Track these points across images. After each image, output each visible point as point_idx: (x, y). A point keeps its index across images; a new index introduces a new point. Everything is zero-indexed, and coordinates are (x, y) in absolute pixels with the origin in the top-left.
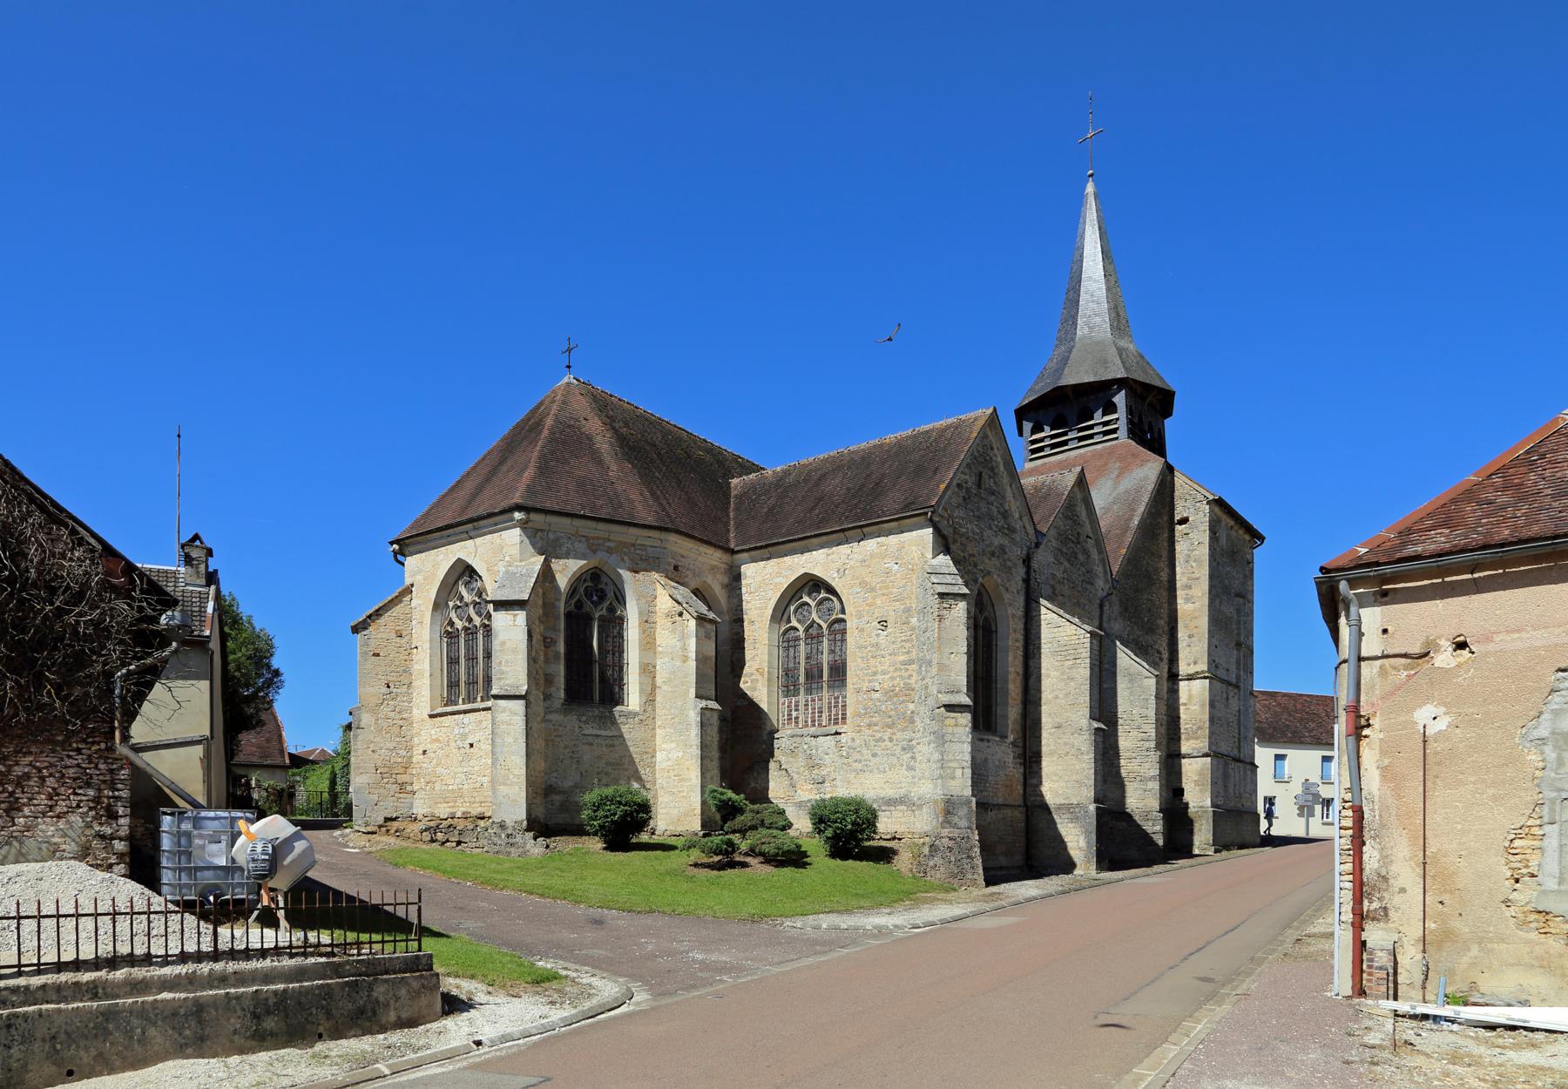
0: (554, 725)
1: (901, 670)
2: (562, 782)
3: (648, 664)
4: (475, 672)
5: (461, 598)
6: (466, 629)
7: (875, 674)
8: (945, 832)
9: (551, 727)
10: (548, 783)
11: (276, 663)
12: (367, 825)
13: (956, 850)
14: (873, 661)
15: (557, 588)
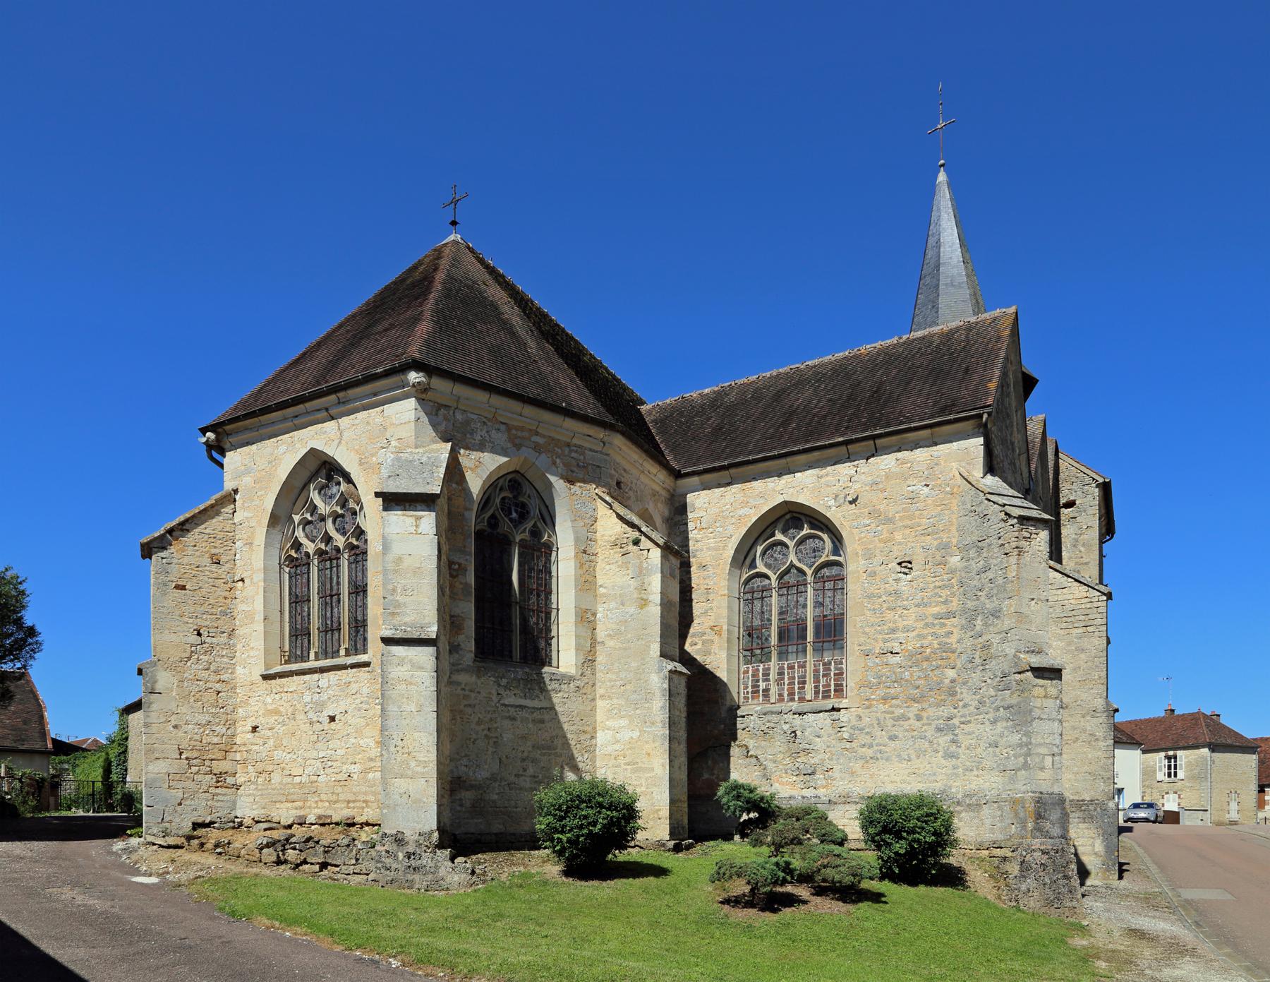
0: (463, 689)
1: (934, 625)
2: (474, 773)
3: (586, 611)
4: (336, 614)
5: (314, 509)
6: (320, 553)
7: (893, 631)
8: (1037, 843)
9: (459, 691)
10: (456, 775)
11: (29, 618)
12: (166, 834)
13: (1050, 869)
14: (889, 615)
15: (466, 491)
